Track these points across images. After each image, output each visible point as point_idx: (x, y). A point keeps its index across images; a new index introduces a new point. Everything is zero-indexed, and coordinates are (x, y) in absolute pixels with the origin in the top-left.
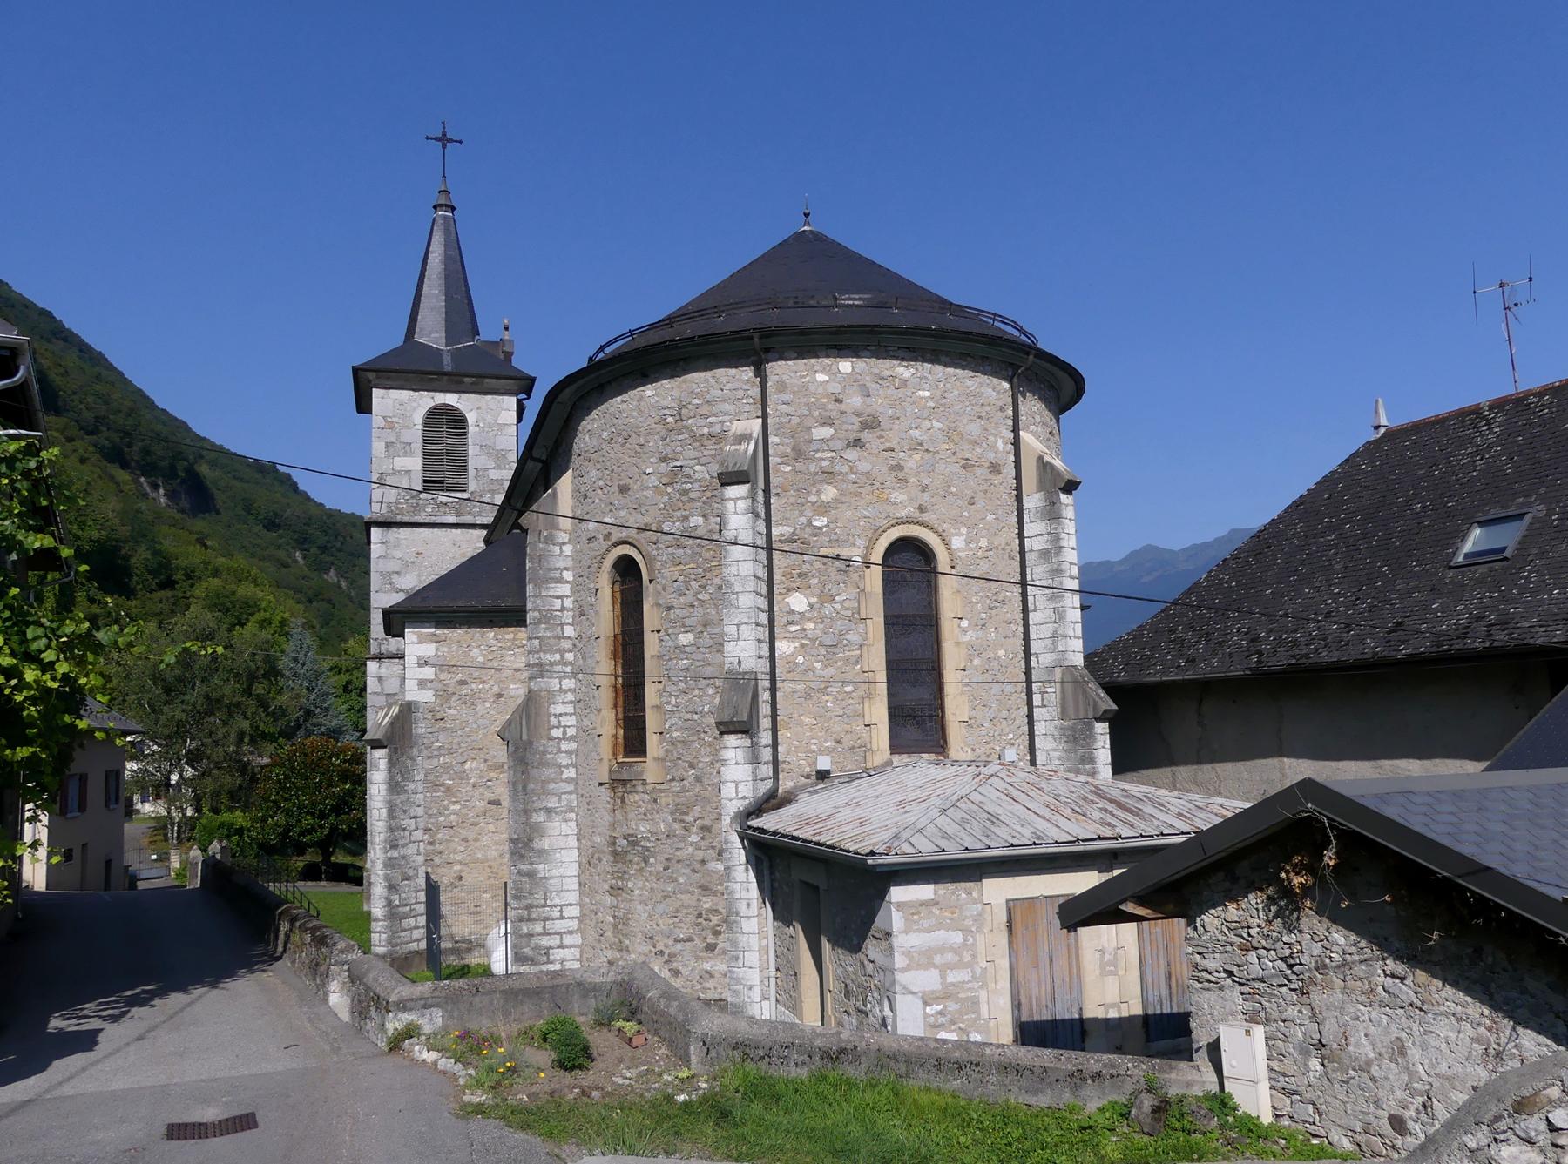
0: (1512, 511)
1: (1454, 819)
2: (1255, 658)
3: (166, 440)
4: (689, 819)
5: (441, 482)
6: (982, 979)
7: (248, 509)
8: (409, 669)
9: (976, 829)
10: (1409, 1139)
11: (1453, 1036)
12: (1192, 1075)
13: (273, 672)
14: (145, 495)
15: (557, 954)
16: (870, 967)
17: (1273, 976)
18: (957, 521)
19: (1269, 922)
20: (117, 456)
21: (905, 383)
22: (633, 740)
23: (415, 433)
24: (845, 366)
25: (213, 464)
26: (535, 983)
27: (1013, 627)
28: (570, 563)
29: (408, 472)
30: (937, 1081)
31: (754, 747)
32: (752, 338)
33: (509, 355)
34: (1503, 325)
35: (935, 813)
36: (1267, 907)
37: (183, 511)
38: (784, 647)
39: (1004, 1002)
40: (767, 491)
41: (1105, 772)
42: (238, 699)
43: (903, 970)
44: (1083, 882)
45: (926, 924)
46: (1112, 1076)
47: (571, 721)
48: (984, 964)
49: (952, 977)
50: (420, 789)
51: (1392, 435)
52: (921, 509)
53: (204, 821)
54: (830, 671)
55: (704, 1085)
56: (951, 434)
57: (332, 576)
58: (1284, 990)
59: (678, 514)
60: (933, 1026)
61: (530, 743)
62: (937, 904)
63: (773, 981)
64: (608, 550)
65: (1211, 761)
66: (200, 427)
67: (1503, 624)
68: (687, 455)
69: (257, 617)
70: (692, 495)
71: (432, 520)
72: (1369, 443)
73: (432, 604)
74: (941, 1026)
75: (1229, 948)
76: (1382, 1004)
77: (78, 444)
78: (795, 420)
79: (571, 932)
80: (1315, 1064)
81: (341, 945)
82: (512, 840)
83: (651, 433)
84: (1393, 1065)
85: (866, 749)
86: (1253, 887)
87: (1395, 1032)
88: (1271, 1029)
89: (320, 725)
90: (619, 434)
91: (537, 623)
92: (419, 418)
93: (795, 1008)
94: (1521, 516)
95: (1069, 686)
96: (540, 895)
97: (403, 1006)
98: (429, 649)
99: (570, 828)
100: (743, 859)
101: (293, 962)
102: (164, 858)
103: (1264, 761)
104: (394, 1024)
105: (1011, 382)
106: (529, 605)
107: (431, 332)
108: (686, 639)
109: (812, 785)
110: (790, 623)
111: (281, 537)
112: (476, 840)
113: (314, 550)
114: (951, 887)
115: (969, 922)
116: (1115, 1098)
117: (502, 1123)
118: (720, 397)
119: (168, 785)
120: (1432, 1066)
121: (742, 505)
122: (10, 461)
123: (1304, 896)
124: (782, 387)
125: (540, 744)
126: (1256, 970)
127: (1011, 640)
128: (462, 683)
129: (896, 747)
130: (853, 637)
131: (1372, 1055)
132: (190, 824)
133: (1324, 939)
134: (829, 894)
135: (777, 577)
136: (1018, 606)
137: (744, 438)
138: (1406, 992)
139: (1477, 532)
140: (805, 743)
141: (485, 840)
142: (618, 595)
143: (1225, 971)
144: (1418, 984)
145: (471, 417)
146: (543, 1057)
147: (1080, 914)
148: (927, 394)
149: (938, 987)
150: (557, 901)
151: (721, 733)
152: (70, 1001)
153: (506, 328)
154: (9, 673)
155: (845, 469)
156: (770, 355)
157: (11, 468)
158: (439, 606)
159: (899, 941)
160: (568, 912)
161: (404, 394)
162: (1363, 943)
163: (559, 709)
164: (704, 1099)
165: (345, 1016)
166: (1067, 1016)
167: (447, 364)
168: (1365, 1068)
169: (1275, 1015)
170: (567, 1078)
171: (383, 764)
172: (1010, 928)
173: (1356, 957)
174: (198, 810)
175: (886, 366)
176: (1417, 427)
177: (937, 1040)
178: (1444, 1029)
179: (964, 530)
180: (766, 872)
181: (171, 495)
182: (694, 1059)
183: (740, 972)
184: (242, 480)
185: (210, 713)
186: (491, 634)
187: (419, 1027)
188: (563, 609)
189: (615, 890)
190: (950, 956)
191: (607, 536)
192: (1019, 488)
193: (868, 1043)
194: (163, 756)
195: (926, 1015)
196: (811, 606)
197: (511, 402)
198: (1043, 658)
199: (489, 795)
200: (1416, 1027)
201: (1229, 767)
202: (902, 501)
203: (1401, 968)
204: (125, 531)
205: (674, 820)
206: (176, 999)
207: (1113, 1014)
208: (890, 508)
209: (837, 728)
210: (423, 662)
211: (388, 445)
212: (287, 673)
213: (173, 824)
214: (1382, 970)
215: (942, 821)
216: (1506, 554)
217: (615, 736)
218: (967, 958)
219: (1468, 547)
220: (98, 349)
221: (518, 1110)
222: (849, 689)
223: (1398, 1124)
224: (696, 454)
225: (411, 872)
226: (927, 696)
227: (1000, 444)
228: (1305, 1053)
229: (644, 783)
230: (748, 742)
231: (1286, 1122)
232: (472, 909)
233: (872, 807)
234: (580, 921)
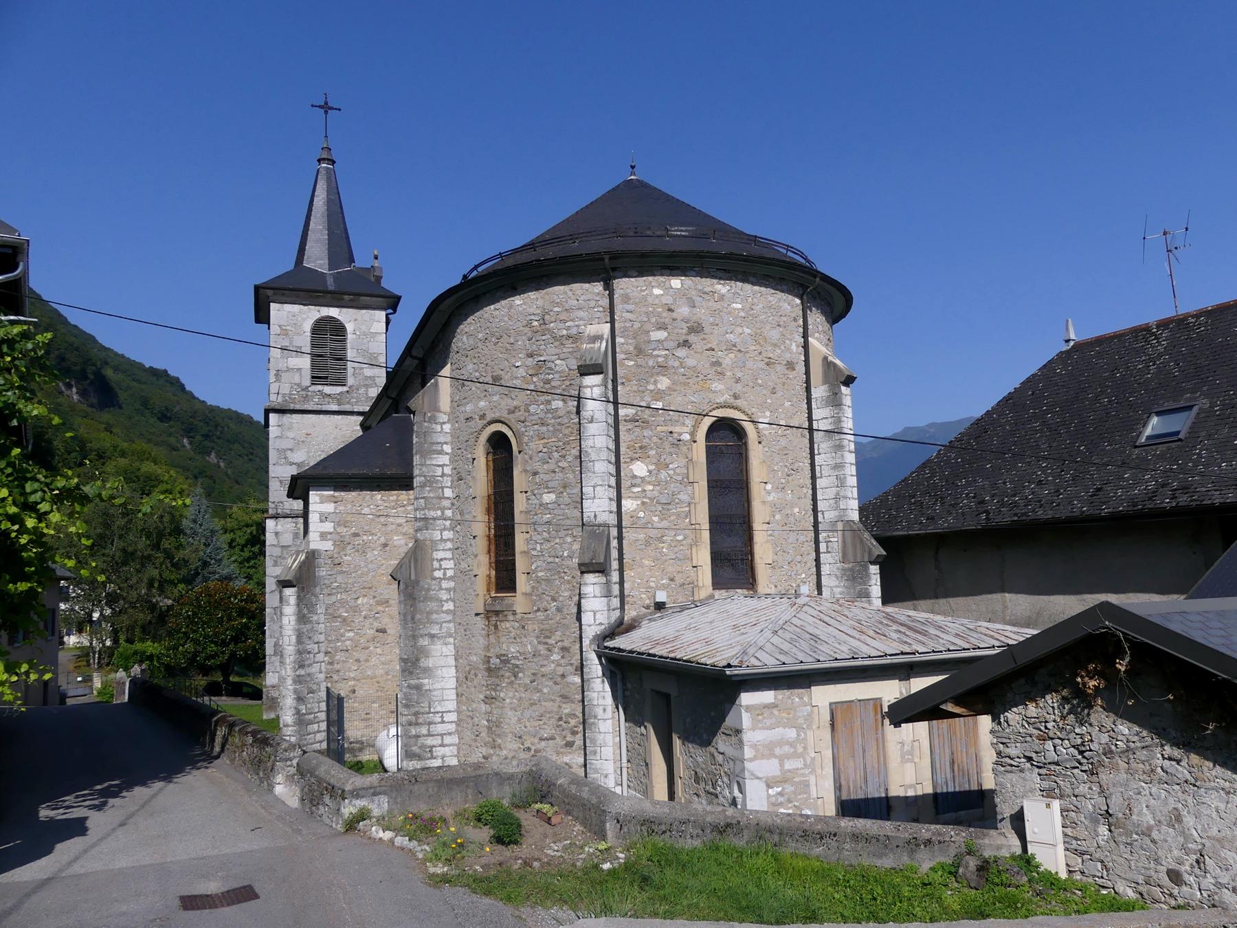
0: (1182, 404)
1: (1223, 633)
2: (984, 516)
3: (77, 349)
6: (811, 766)
9: (805, 646)
10: (1184, 888)
11: (1222, 806)
12: (1001, 841)
13: (178, 531)
14: (61, 393)
15: (439, 751)
16: (720, 758)
17: (1067, 760)
18: (763, 406)
19: (1063, 718)
21: (722, 297)
22: (505, 578)
24: (676, 282)
25: (116, 369)
26: (461, 774)
27: (805, 490)
28: (449, 439)
29: (299, 370)
30: (803, 848)
31: (608, 583)
32: (603, 259)
33: (379, 279)
34: (1166, 265)
35: (768, 634)
36: (1062, 706)
37: (92, 406)
38: (628, 505)
39: (829, 784)
40: (615, 381)
41: (877, 602)
42: (149, 552)
43: (751, 760)
44: (890, 691)
45: (768, 722)
46: (940, 842)
47: (450, 564)
48: (813, 754)
49: (789, 765)
50: (322, 620)
51: (1079, 347)
52: (736, 397)
53: (121, 650)
54: (665, 524)
55: (622, 856)
56: (758, 338)
57: (213, 458)
58: (1076, 771)
60: (773, 804)
61: (417, 582)
62: (776, 706)
63: (625, 771)
65: (946, 596)
67: (1185, 488)
68: (549, 351)
70: (553, 384)
71: (319, 408)
73: (331, 471)
74: (781, 804)
75: (1028, 739)
76: (1160, 781)
78: (637, 325)
79: (450, 734)
80: (1103, 830)
83: (519, 334)
84: (1171, 830)
85: (694, 586)
86: (1048, 689)
87: (1172, 803)
88: (1066, 803)
89: (214, 573)
90: (493, 335)
91: (423, 486)
93: (646, 791)
94: (1190, 408)
95: (848, 534)
96: (426, 704)
97: (357, 794)
98: (329, 507)
99: (449, 650)
100: (600, 673)
101: (232, 761)
102: (88, 680)
103: (989, 596)
104: (349, 808)
105: (801, 299)
106: (416, 472)
107: (317, 258)
108: (549, 498)
109: (651, 614)
110: (634, 486)
111: (171, 427)
112: (367, 661)
113: (198, 438)
114: (787, 692)
115: (801, 721)
116: (943, 859)
117: (467, 890)
118: (577, 305)
119: (91, 621)
120: (1204, 830)
121: (597, 392)
122: (11, 342)
123: (1095, 697)
124: (626, 299)
126: (1052, 756)
128: (356, 535)
129: (717, 584)
130: (683, 497)
131: (1152, 822)
132: (110, 652)
133: (1110, 730)
134: (681, 700)
135: (623, 449)
137: (597, 338)
138: (1182, 772)
139: (1155, 420)
140: (645, 579)
141: (374, 660)
142: (491, 464)
143: (1025, 757)
144: (1191, 765)
145: (349, 327)
146: (484, 834)
147: (902, 713)
148: (740, 306)
149: (778, 773)
150: (439, 709)
151: (582, 573)
152: (53, 795)
153: (376, 258)
154: (13, 519)
156: (616, 274)
157: (12, 348)
158: (336, 474)
159: (748, 736)
160: (447, 717)
161: (296, 308)
162: (1145, 733)
163: (440, 555)
164: (627, 867)
165: (293, 802)
166: (877, 795)
167: (331, 284)
168: (1147, 833)
169: (1068, 791)
170: (506, 853)
171: (293, 600)
172: (833, 726)
173: (1138, 744)
174: (116, 641)
175: (707, 284)
176: (1100, 341)
177: (801, 815)
178: (1214, 800)
180: (619, 684)
181: (83, 393)
182: (610, 834)
184: (139, 381)
185: (125, 563)
186: (378, 496)
187: (369, 811)
188: (443, 475)
189: (488, 700)
190: (786, 748)
192: (808, 381)
193: (748, 819)
194: (87, 598)
195: (769, 796)
196: (650, 472)
197: (381, 315)
198: (828, 515)
199: (376, 625)
200: (1190, 800)
201: (960, 600)
202: (720, 390)
203: (1177, 753)
205: (539, 643)
206: (139, 791)
207: (911, 793)
208: (711, 395)
209: (670, 569)
210: (324, 518)
212: (188, 532)
213: (94, 653)
214: (1160, 755)
215: (775, 640)
216: (1181, 436)
217: (489, 576)
218: (800, 750)
219: (1148, 431)
221: (478, 880)
222: (680, 538)
223: (1175, 877)
224: (557, 351)
225: (315, 687)
226: (739, 544)
227: (794, 347)
228: (1095, 822)
229: (514, 613)
230: (603, 580)
231: (1078, 877)
232: (364, 716)
233: (710, 631)
234: (458, 725)
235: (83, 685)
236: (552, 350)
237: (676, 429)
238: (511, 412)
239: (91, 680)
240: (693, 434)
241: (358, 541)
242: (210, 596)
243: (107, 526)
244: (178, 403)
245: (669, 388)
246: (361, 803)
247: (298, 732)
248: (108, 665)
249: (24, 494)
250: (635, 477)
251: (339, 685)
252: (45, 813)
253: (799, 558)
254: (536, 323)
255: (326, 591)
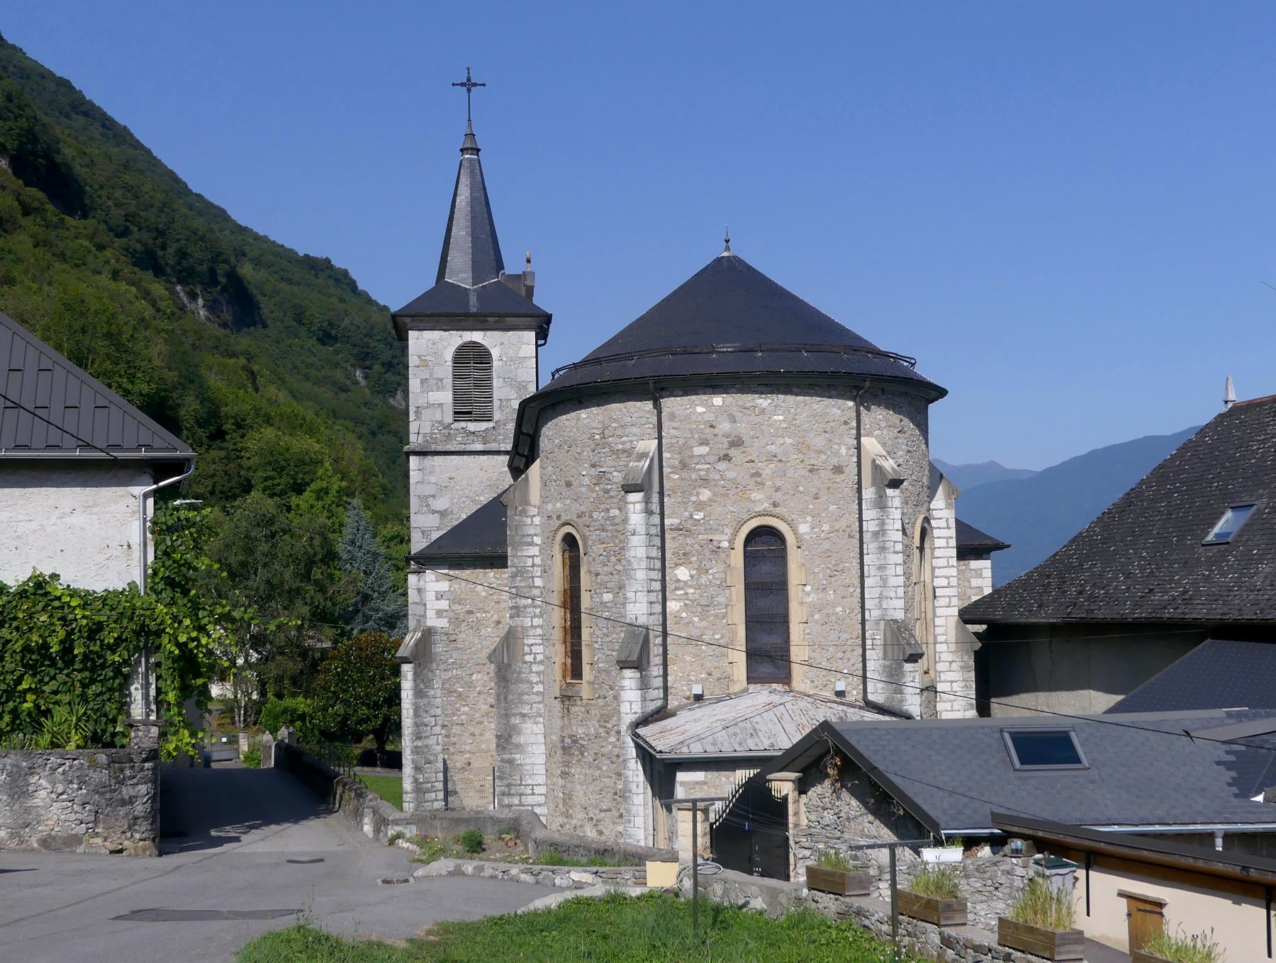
4: (609, 725)
5: (470, 413)
7: (299, 318)
8: (431, 594)
13: (330, 556)
18: (803, 513)
20: (149, 261)
21: (763, 411)
23: (446, 370)
24: (718, 400)
25: (257, 262)
27: (851, 589)
29: (441, 405)
33: (530, 291)
38: (672, 606)
42: (298, 584)
52: (775, 505)
53: (268, 706)
54: (704, 624)
59: (603, 506)
61: (509, 665)
64: (559, 528)
66: (240, 216)
68: (608, 464)
69: (314, 486)
71: (462, 448)
72: (1220, 415)
77: (108, 253)
78: (682, 441)
79: (540, 805)
81: (370, 797)
82: (497, 737)
89: (377, 611)
92: (449, 355)
98: (444, 586)
99: (539, 729)
102: (233, 741)
104: (391, 831)
107: (460, 275)
108: (607, 597)
110: (677, 589)
111: (337, 352)
112: (481, 735)
113: (377, 368)
114: (716, 774)
124: (672, 417)
125: (517, 666)
127: (848, 600)
128: (470, 612)
129: (751, 679)
130: (721, 599)
135: (668, 555)
136: (856, 573)
139: (1229, 514)
140: (687, 674)
142: (567, 561)
145: (495, 353)
148: (781, 418)
150: (529, 782)
152: (219, 825)
153: (529, 261)
155: (717, 477)
156: (663, 393)
160: (538, 790)
161: (436, 335)
165: (371, 835)
171: (410, 676)
174: (263, 694)
179: (809, 519)
181: (212, 307)
182: (530, 850)
183: (631, 831)
184: (289, 281)
189: (564, 775)
191: (559, 517)
196: (692, 576)
198: (873, 614)
202: (760, 499)
204: (172, 376)
208: (750, 505)
209: (708, 665)
210: (440, 596)
211: (423, 381)
213: (239, 708)
217: (565, 664)
220: (122, 123)
225: (432, 758)
227: (843, 450)
235: (226, 747)
236: (610, 461)
237: (715, 537)
238: (579, 516)
239: (237, 742)
240: (731, 541)
241: (471, 618)
242: (361, 649)
243: (250, 551)
244: (346, 313)
245: (710, 500)
246: (398, 829)
247: (417, 799)
248: (255, 724)
249: (198, 619)
250: (678, 581)
251: (454, 757)
252: (213, 833)
253: (841, 655)
254: (597, 437)
255: (442, 667)
